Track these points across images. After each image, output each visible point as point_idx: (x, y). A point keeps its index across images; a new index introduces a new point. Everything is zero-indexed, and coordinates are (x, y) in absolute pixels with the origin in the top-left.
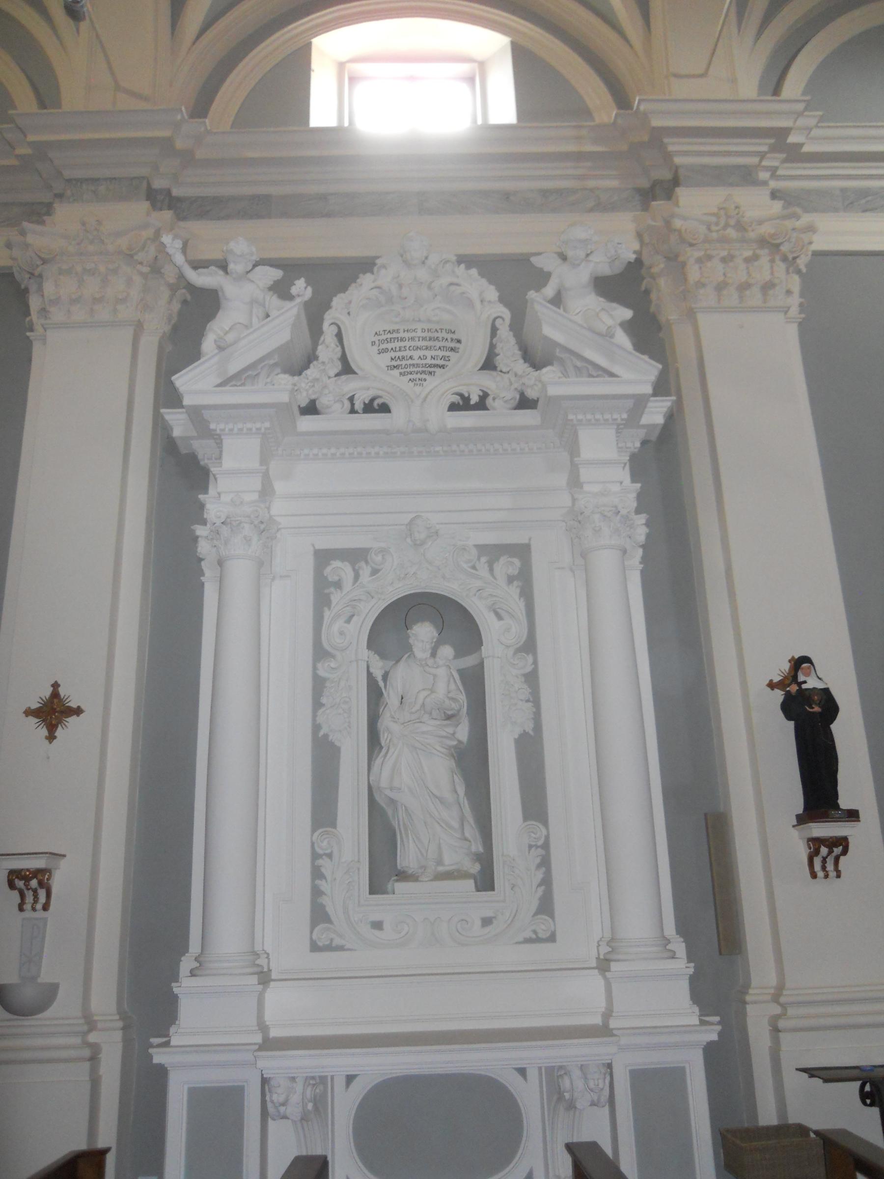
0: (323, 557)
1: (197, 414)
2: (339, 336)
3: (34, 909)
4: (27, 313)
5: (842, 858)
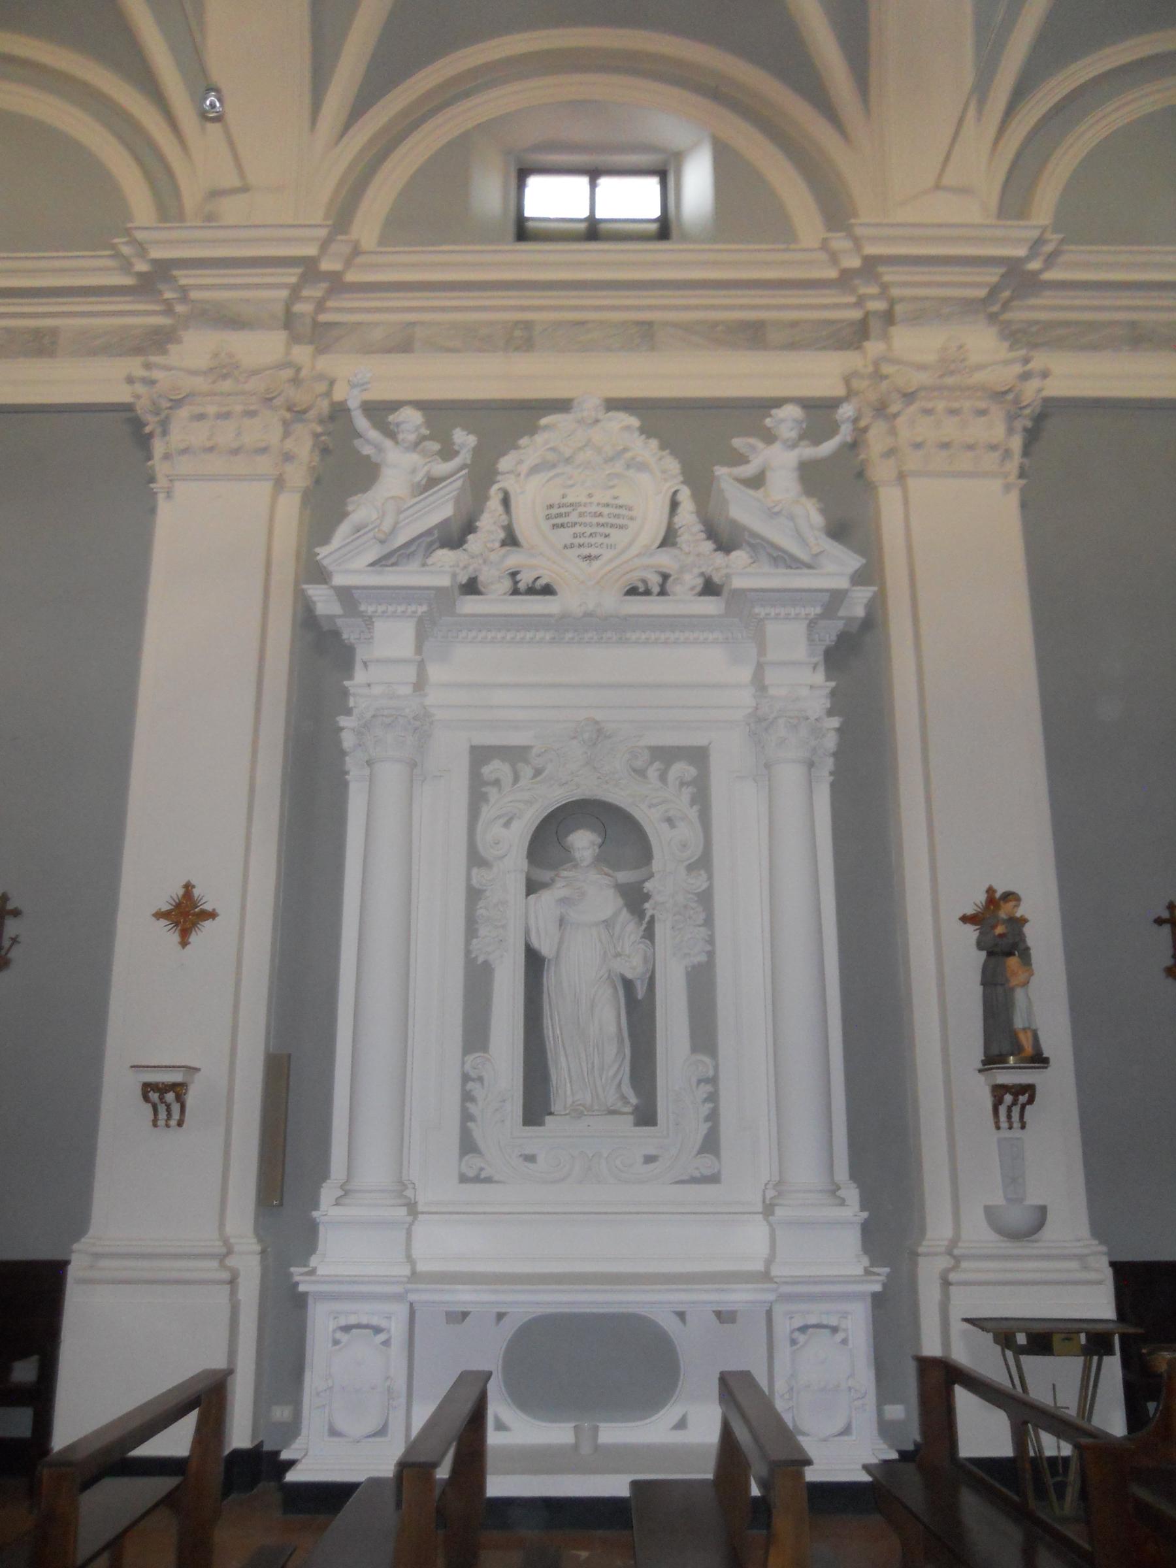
0: (480, 755)
1: (346, 595)
2: (506, 502)
3: (168, 1126)
4: (149, 457)
5: (1027, 1107)
